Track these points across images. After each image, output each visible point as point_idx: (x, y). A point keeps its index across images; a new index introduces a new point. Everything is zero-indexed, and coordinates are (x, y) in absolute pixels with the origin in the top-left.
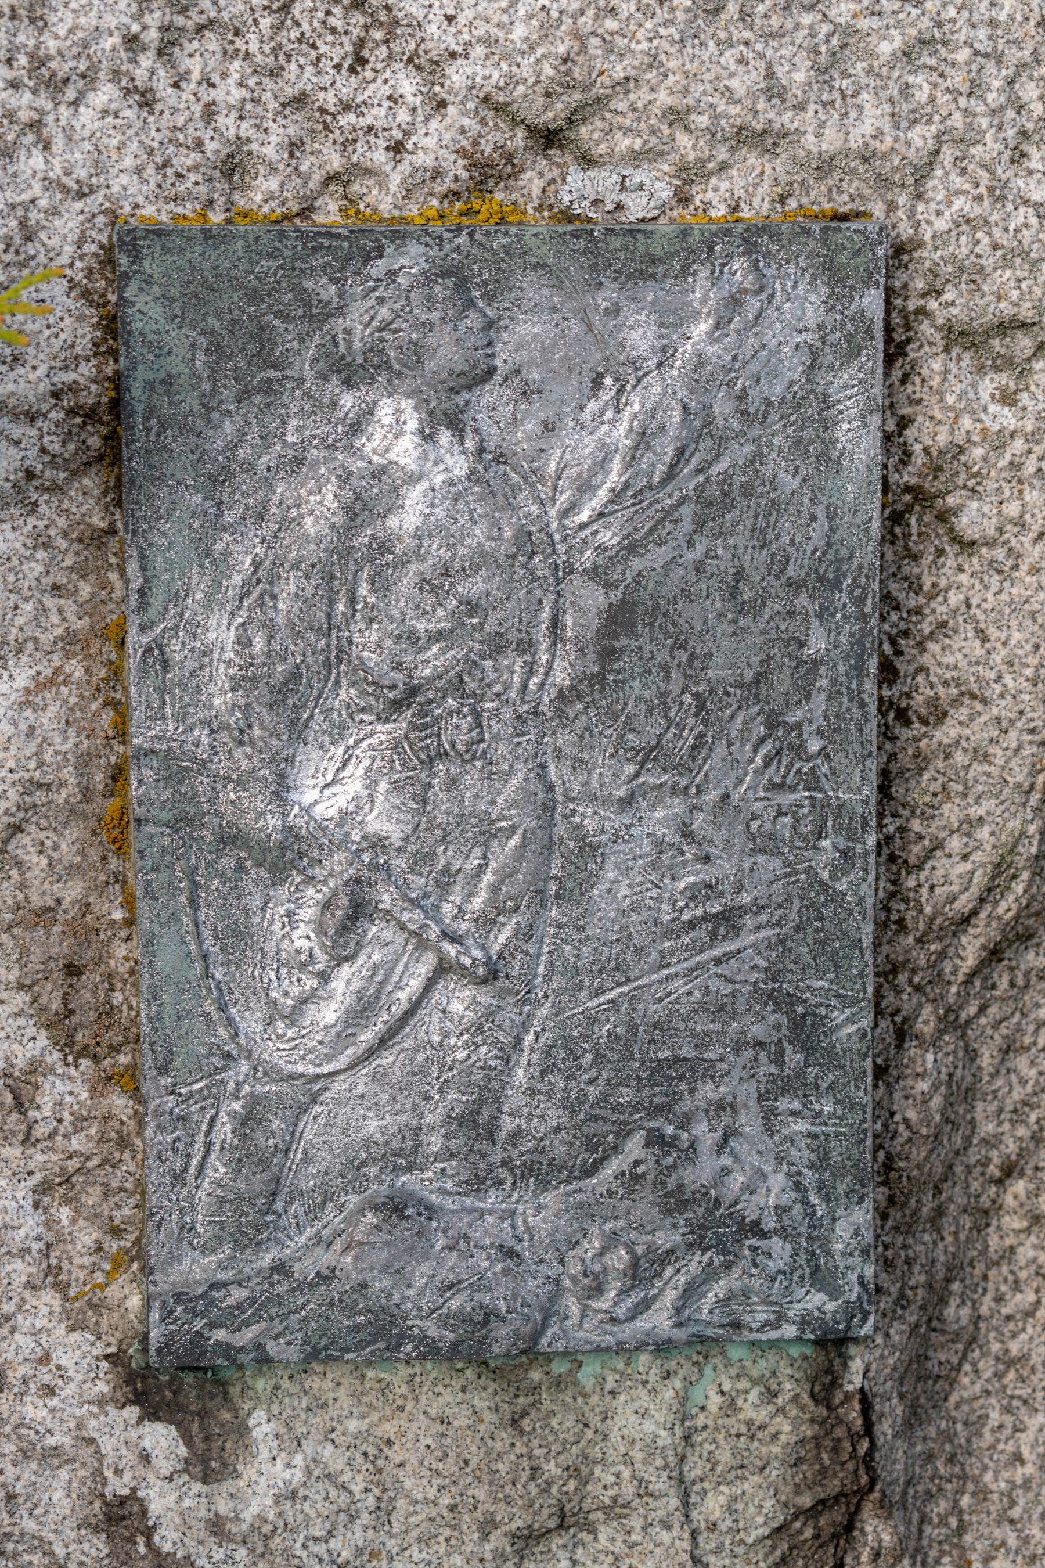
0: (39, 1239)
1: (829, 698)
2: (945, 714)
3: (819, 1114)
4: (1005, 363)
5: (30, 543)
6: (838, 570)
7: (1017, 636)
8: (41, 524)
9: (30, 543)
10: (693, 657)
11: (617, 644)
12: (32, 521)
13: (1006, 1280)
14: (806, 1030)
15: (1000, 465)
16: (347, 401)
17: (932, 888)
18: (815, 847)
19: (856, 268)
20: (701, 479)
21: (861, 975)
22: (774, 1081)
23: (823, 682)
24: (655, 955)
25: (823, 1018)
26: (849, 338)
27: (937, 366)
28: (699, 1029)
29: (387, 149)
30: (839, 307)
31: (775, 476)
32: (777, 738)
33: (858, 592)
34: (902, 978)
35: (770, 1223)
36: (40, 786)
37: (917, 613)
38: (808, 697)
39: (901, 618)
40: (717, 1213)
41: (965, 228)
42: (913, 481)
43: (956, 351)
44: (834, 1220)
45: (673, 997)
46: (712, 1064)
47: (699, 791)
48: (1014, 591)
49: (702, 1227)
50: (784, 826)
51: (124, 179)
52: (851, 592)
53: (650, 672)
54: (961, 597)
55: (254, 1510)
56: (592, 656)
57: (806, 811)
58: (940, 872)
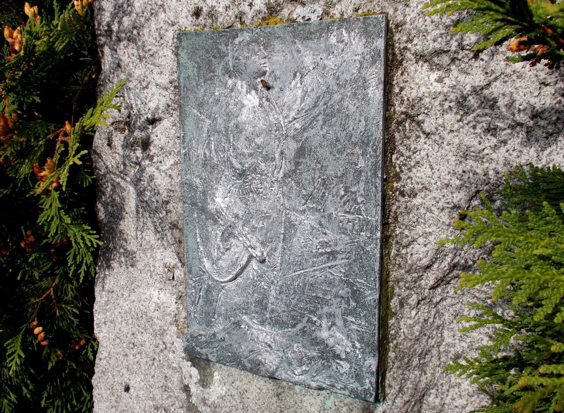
0: (173, 312)
1: (365, 184)
2: (416, 194)
3: (360, 324)
4: (439, 67)
5: (172, 124)
6: (368, 139)
7: (442, 168)
8: (173, 119)
9: (172, 124)
10: (322, 166)
11: (300, 161)
12: (172, 118)
13: (456, 394)
14: (356, 295)
15: (435, 104)
16: (230, 82)
17: (412, 254)
18: (360, 234)
19: (375, 32)
20: (325, 106)
21: (374, 280)
22: (347, 310)
23: (363, 178)
24: (311, 262)
25: (362, 292)
26: (372, 57)
27: (412, 68)
28: (324, 288)
29: (248, 5)
30: (369, 46)
31: (348, 106)
32: (348, 196)
33: (375, 147)
34: (401, 284)
35: (343, 356)
36: (171, 191)
37: (409, 158)
38: (358, 183)
39: (404, 160)
40: (327, 349)
41: (421, 15)
42: (404, 110)
43: (420, 63)
44: (365, 360)
45: (316, 277)
46: (327, 301)
47: (324, 211)
48: (443, 151)
49: (322, 352)
50: (350, 226)
51: (183, 20)
52: (372, 147)
53: (309, 170)
54: (425, 153)
55: (213, 399)
56: (293, 164)
57: (357, 222)
58: (415, 250)
